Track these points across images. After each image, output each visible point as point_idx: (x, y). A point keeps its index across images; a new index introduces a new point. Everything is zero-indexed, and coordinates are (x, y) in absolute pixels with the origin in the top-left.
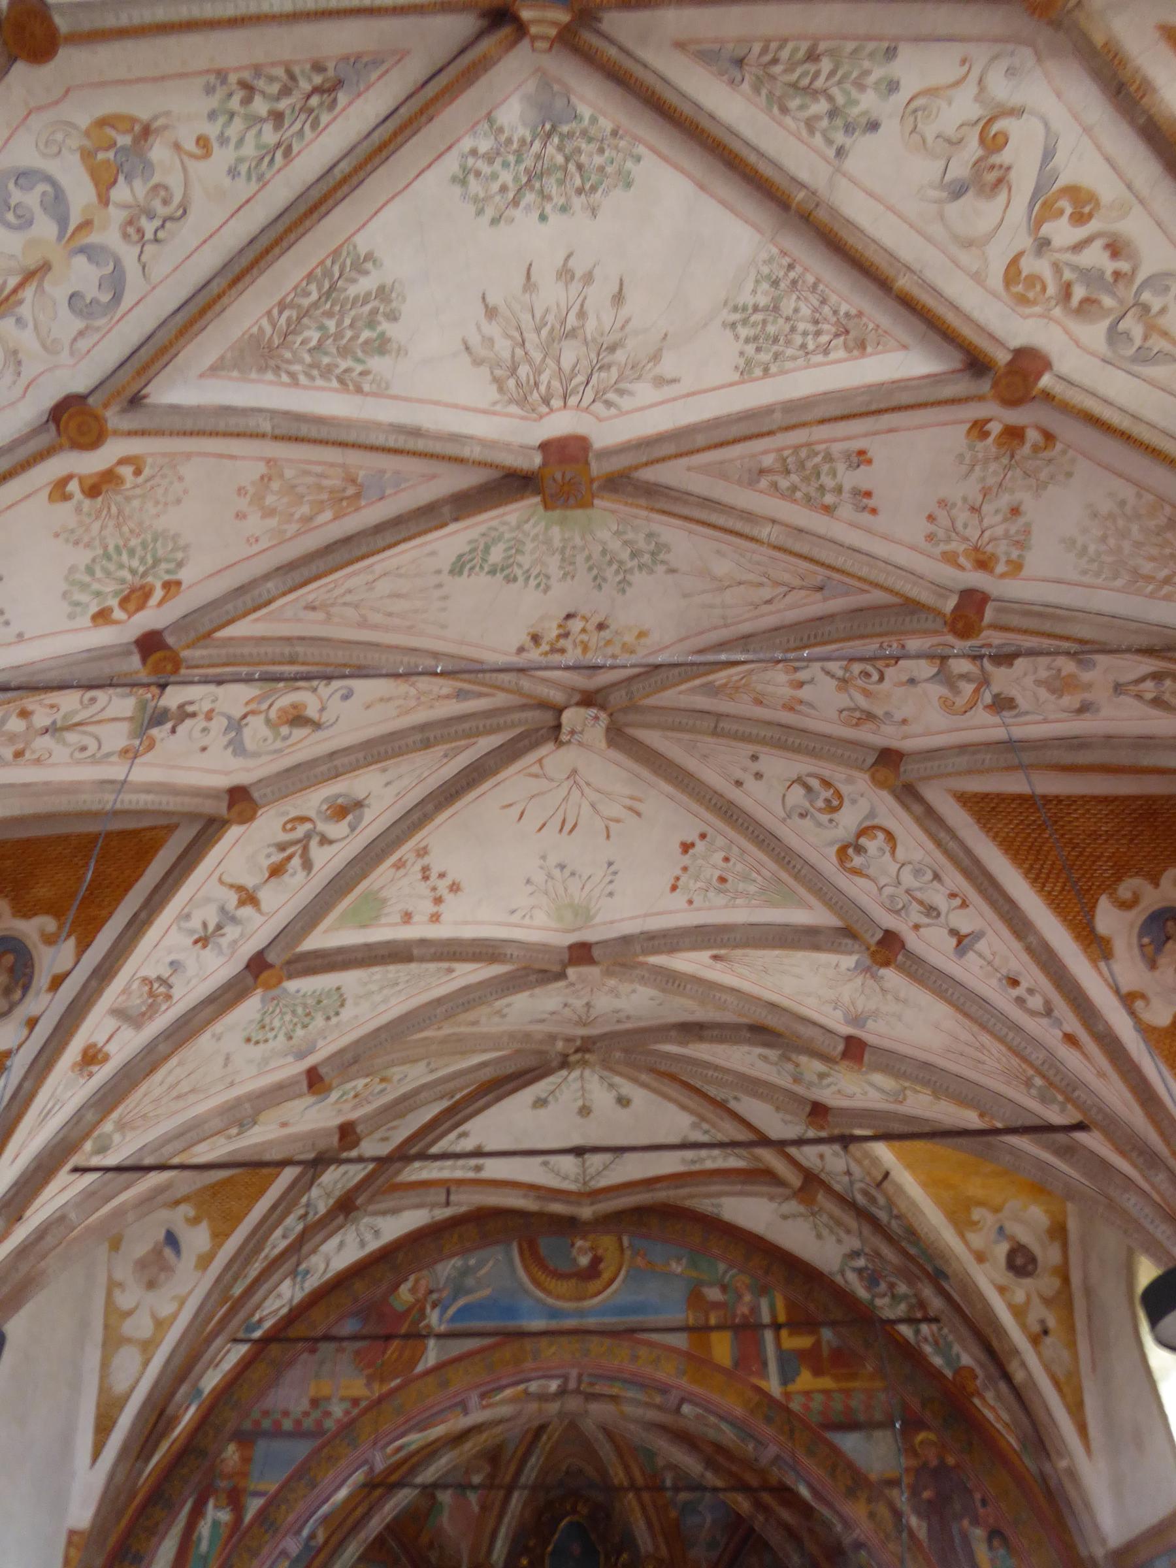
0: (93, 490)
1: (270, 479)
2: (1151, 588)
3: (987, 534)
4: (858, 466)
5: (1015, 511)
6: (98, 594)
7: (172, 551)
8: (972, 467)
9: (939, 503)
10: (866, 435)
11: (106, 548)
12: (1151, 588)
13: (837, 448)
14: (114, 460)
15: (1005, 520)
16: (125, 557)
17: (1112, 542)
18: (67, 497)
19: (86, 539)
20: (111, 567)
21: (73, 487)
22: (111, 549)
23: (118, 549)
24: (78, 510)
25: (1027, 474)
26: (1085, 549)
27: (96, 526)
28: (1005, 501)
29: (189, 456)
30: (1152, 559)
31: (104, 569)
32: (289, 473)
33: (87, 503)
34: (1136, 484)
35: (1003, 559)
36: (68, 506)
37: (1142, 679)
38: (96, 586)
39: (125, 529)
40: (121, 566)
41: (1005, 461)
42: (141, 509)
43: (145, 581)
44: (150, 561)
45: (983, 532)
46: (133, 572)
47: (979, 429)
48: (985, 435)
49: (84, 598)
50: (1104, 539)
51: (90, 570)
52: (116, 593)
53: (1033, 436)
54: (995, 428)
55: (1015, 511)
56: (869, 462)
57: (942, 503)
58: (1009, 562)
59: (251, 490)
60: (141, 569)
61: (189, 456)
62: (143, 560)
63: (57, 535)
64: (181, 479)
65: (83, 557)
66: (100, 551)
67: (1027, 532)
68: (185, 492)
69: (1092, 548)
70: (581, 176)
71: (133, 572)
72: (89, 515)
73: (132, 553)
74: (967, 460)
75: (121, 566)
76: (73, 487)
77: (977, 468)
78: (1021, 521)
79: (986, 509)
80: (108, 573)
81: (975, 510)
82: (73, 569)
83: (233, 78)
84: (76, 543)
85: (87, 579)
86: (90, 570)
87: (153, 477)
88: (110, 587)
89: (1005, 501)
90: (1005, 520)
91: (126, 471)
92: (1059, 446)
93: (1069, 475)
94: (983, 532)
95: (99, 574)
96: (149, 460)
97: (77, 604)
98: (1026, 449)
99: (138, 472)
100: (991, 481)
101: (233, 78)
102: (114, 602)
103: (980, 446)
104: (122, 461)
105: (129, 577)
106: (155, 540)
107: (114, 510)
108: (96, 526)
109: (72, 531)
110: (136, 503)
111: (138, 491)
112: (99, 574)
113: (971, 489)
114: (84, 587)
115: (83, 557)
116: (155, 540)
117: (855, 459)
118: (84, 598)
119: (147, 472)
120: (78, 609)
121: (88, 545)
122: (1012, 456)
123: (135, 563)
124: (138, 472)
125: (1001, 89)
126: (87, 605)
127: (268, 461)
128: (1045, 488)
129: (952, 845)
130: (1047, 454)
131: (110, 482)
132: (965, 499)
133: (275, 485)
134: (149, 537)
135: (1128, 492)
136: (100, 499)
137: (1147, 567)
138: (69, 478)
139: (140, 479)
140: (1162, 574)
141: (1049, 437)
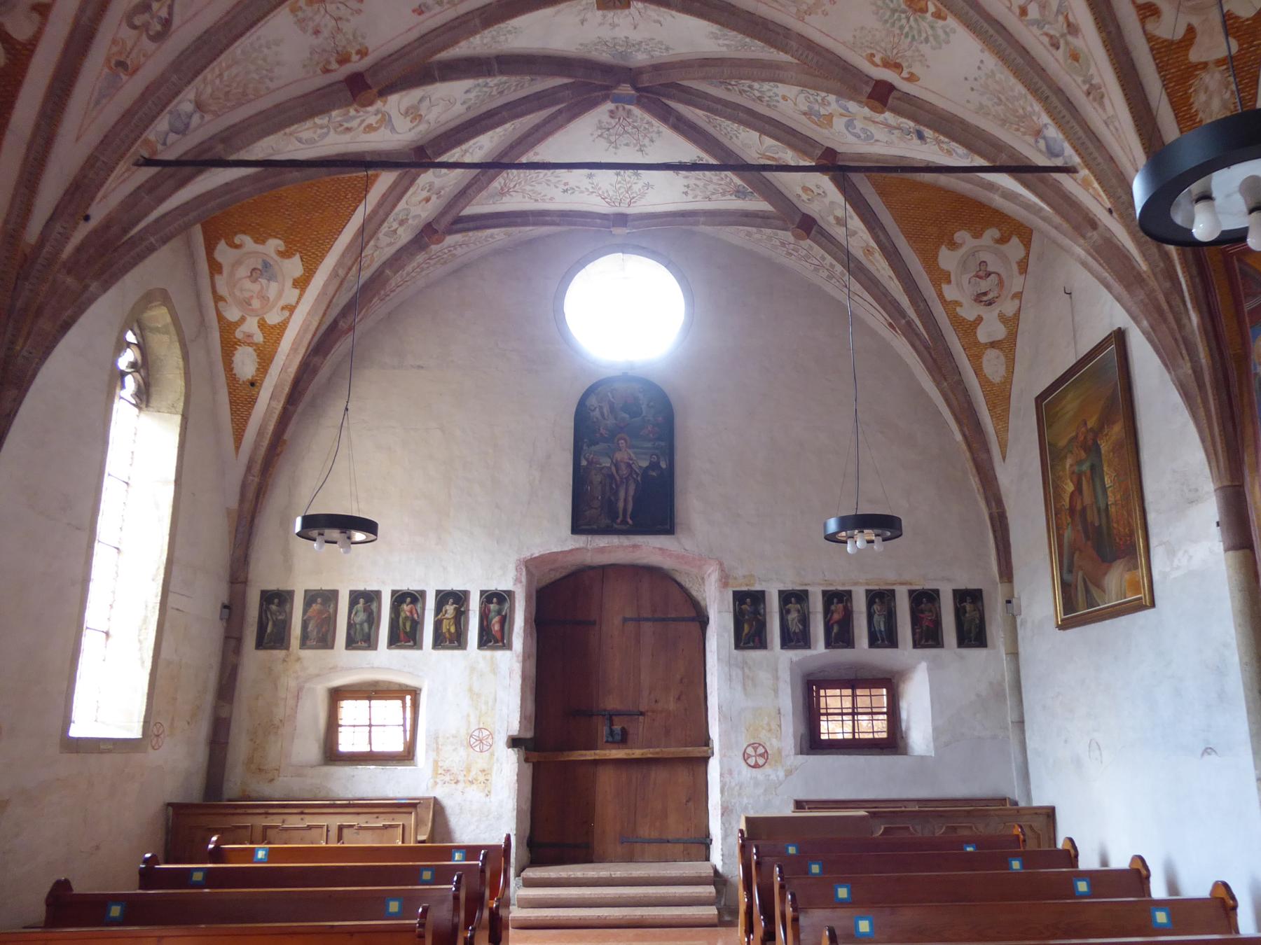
0: (897, 67)
1: (805, 12)
2: (224, 65)
3: (322, 11)
4: (420, 6)
5: (317, 32)
6: (932, 27)
7: (882, 9)
8: (354, 36)
9: (361, 10)
10: (423, 22)
11: (911, 43)
12: (224, 65)
13: (437, 9)
14: (880, 68)
15: (319, 25)
16: (907, 29)
17: (260, 62)
18: (912, 74)
19: (917, 54)
20: (915, 33)
21: (905, 74)
22: (909, 39)
23: (907, 36)
24: (910, 66)
25: (324, 50)
26: (269, 48)
27: (909, 53)
28: (326, 33)
29: (844, 43)
30: (236, 76)
31: (920, 35)
32: (794, 10)
33: (904, 65)
34: (274, 91)
35: (304, 7)
36: (913, 70)
37: (170, 13)
38: (930, 32)
39: (896, 40)
40: (911, 27)
41: (340, 49)
42: (883, 40)
43: (907, 8)
44: (896, 15)
45: (326, 11)
46: (908, 19)
47: (363, 53)
48: (359, 52)
49: (940, 32)
50: (265, 60)
51: (927, 40)
52: (924, 19)
53: (334, 66)
54: (355, 58)
55: (317, 32)
56: (414, 11)
57: (359, 11)
58: (301, 8)
59: (820, 11)
60: (903, 16)
61: (844, 43)
62: (900, 20)
63: (928, 66)
64: (854, 37)
65: (924, 48)
66: (915, 43)
67: (304, 30)
68: (856, 30)
69: (265, 50)
70: (629, 546)
71: (908, 19)
72: (907, 61)
73: (902, 28)
74: (360, 39)
75: (911, 27)
76: (905, 74)
77: (351, 37)
78: (310, 31)
79: (334, 22)
80: (920, 32)
81: (338, 19)
82: (933, 48)
83: (765, 104)
84: (923, 56)
85: (931, 39)
86: (927, 40)
87: (868, 47)
88: (924, 25)
89: (326, 33)
90: (319, 25)
91: (877, 60)
92: (319, 72)
93: (305, 66)
94: (326, 11)
95: (924, 35)
96: (864, 54)
97: (946, 33)
98: (333, 60)
99: (873, 55)
100: (339, 37)
101: (765, 104)
102: (928, 15)
103: (358, 47)
104: (877, 65)
105: (912, 19)
106: (886, 21)
107: (895, 51)
108: (909, 53)
109: (920, 61)
110: (883, 44)
111: (878, 48)
112: (924, 35)
113: (347, 27)
114: (936, 37)
115: (924, 48)
116: (886, 21)
117: (423, 9)
118: (940, 32)
119: (869, 51)
120: (948, 30)
121: (918, 50)
122: (338, 53)
123: (904, 22)
124: (873, 55)
125: (423, 127)
126: (942, 27)
127: (803, 20)
128: (311, 53)
129: (381, 212)
130: (321, 65)
131: (888, 63)
132: (348, 20)
133: (805, 7)
134: (888, 25)
135: (272, 85)
136: (897, 61)
137: (234, 71)
138: (903, 78)
139: (874, 52)
140: (226, 74)
141: (326, 71)
